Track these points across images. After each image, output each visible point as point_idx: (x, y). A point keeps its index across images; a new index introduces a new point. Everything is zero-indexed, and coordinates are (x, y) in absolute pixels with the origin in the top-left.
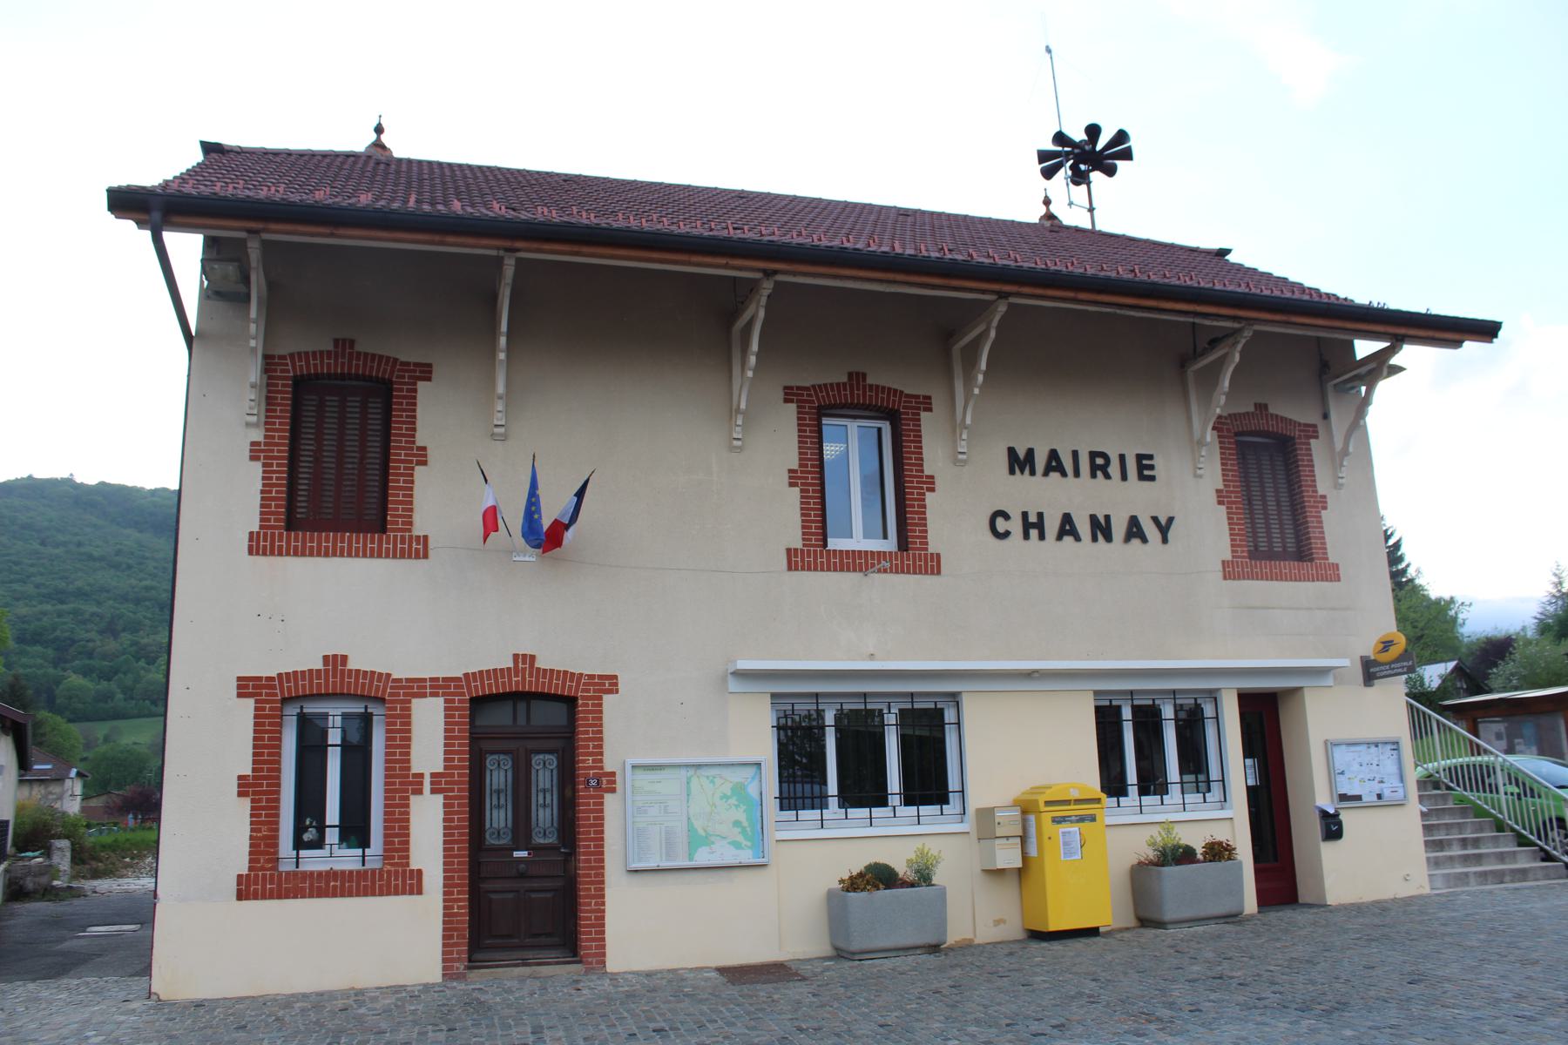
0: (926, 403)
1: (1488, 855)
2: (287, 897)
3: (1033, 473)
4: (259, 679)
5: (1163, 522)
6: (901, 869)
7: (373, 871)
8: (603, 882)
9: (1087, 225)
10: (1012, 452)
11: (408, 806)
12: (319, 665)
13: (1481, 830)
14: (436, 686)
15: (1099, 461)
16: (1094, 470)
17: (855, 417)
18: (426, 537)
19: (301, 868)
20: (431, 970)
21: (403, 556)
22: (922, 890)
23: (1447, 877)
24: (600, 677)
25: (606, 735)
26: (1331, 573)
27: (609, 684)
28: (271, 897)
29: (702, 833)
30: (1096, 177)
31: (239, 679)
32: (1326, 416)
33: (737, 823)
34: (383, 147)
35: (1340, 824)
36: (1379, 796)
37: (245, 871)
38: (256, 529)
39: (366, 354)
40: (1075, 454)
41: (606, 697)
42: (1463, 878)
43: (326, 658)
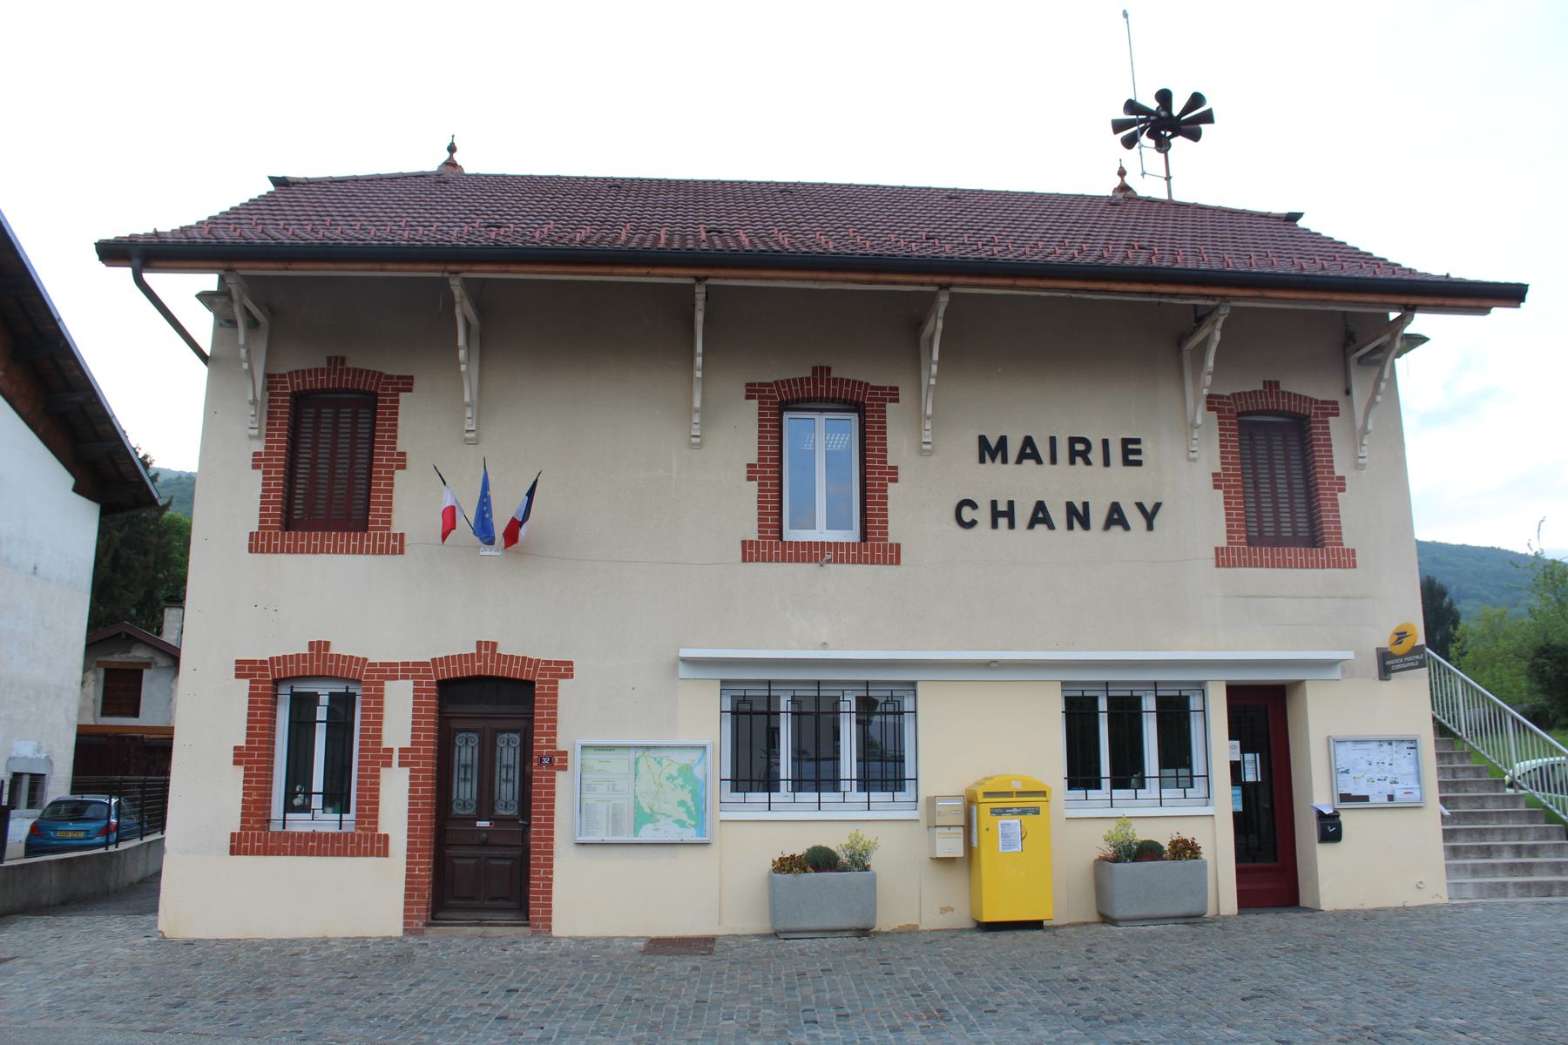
0: (893, 394)
1: (1541, 865)
2: (272, 854)
3: (1005, 461)
5: (1149, 508)
10: (983, 440)
11: (378, 777)
13: (1548, 837)
15: (1080, 447)
16: (1073, 455)
17: (822, 410)
18: (402, 535)
19: (288, 829)
20: (395, 927)
21: (381, 553)
22: (854, 876)
23: (1479, 887)
24: (557, 662)
25: (560, 717)
26: (1347, 559)
27: (564, 669)
29: (647, 810)
30: (1179, 142)
32: (1348, 392)
33: (682, 803)
35: (1339, 826)
36: (1391, 798)
37: (237, 830)
39: (355, 370)
40: (1053, 440)
41: (561, 682)
42: (1501, 889)
43: (311, 644)
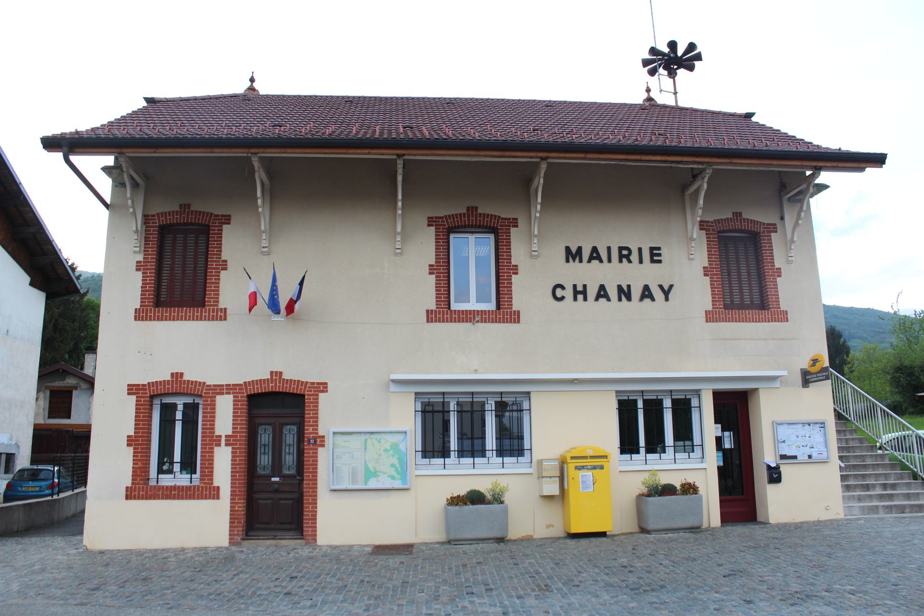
0: (514, 223)
1: (898, 495)
2: (150, 499)
3: (581, 261)
4: (139, 385)
5: (666, 288)
6: (489, 496)
7: (194, 487)
8: (316, 496)
9: (671, 103)
10: (568, 249)
12: (169, 378)
13: (902, 479)
14: (229, 389)
15: (625, 252)
17: (473, 233)
18: (225, 309)
19: (160, 484)
21: (213, 320)
22: (495, 507)
24: (318, 383)
26: (783, 317)
27: (322, 387)
28: (142, 499)
29: (372, 470)
30: (682, 73)
31: (129, 385)
32: (782, 218)
33: (393, 465)
34: (254, 89)
35: (780, 474)
36: (810, 457)
38: (138, 307)
39: (196, 212)
40: (609, 249)
42: (875, 509)
43: (172, 374)
